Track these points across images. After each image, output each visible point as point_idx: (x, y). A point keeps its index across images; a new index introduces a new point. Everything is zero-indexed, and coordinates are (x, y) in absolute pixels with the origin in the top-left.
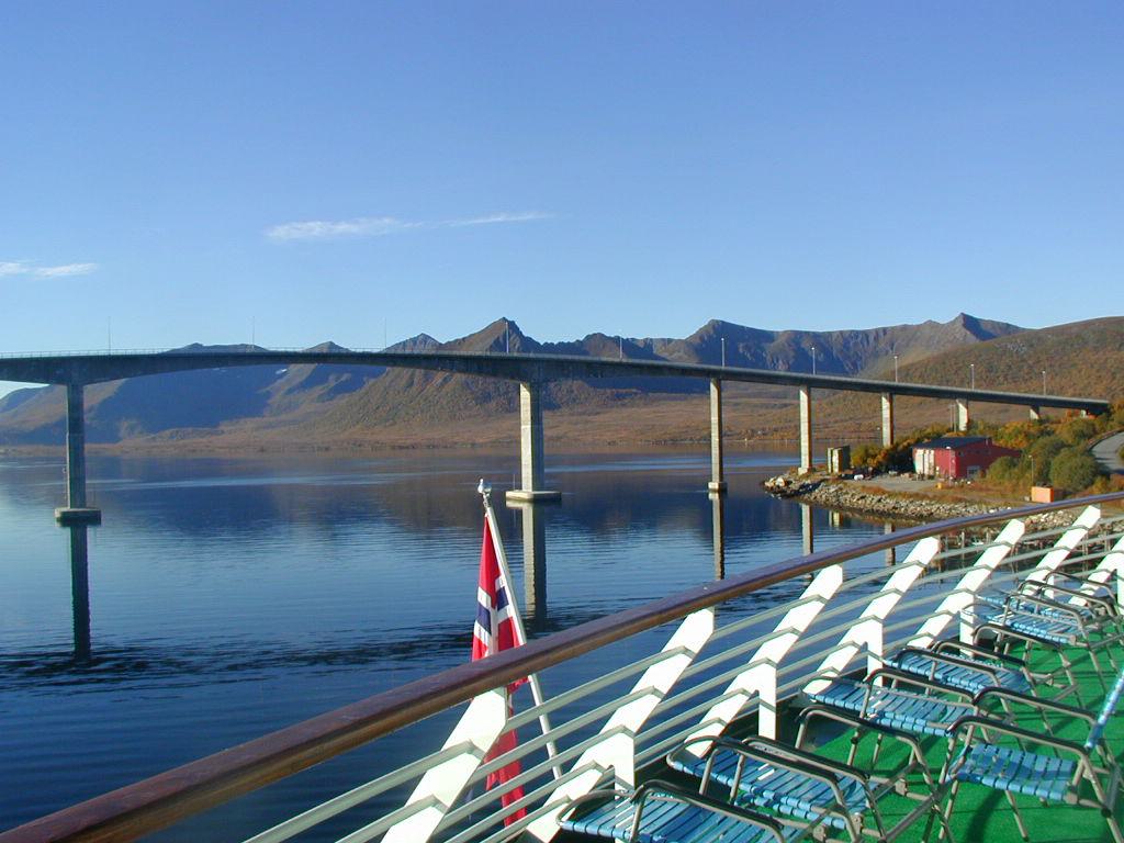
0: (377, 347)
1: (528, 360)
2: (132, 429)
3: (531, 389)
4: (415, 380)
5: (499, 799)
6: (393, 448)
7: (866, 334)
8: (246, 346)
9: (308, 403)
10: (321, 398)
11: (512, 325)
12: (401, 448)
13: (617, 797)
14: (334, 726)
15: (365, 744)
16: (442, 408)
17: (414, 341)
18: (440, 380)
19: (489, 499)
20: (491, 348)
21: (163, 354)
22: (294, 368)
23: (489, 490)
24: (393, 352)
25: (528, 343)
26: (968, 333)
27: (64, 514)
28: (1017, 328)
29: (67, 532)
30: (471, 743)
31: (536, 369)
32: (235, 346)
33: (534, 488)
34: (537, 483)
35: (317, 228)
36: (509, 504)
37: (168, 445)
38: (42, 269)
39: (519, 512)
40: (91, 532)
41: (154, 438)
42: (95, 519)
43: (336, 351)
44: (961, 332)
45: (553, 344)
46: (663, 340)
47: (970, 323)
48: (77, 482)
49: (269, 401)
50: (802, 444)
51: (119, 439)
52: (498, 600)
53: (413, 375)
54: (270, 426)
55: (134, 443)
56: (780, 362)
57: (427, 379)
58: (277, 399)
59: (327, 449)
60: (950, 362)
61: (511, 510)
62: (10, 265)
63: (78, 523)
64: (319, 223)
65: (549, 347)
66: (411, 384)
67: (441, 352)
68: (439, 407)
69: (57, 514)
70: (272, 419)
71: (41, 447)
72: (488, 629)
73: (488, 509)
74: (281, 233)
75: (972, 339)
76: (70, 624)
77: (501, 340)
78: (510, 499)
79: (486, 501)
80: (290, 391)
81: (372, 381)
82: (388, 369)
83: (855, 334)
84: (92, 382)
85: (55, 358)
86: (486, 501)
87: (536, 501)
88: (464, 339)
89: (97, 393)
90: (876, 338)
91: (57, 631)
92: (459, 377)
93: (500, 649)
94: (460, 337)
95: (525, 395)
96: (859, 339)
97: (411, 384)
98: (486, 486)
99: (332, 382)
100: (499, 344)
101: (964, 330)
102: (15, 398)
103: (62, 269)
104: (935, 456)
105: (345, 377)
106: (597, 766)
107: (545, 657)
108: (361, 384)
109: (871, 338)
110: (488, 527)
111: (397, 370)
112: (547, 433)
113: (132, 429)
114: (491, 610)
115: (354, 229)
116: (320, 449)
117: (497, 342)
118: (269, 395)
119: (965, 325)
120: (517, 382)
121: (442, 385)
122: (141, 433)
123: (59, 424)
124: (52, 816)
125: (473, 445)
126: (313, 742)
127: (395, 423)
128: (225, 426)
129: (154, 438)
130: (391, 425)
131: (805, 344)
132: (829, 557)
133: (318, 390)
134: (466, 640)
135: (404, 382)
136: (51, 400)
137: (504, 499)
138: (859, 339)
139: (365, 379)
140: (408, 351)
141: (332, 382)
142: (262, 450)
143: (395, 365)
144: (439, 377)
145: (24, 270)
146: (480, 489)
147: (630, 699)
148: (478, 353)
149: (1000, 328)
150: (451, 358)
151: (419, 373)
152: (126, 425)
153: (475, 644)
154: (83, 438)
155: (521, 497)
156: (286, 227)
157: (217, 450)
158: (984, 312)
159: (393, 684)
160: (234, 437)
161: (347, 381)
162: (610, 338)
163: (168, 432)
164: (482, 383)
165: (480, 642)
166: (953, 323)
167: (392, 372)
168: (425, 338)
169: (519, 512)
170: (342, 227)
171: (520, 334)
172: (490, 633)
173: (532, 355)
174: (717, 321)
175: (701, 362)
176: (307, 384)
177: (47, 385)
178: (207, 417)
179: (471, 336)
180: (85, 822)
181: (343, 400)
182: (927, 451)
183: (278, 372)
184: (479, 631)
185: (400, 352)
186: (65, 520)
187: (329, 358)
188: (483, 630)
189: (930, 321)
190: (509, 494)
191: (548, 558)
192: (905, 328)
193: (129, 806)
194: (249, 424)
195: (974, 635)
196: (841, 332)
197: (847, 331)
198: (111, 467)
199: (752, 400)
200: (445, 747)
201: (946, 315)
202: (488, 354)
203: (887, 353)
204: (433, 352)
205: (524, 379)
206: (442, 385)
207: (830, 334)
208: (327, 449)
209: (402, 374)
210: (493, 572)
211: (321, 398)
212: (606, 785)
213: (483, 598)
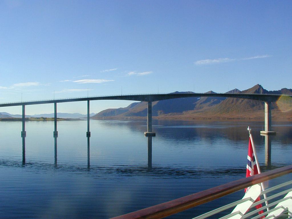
0: (224, 92)
1: (266, 96)
2: (161, 113)
3: (268, 104)
4: (234, 101)
5: (258, 213)
6: (228, 119)
8: (190, 92)
9: (206, 107)
10: (209, 106)
11: (260, 86)
12: (230, 119)
13: (289, 217)
14: (217, 191)
15: (230, 194)
16: (241, 108)
17: (234, 90)
18: (241, 101)
19: (250, 132)
20: (255, 92)
21: (169, 94)
22: (202, 98)
23: (251, 129)
24: (228, 93)
25: (265, 91)
27: (147, 133)
29: (147, 138)
30: (251, 198)
31: (269, 98)
32: (187, 92)
33: (268, 131)
34: (269, 129)
35: (207, 61)
36: (261, 135)
37: (170, 117)
38: (139, 73)
39: (264, 137)
40: (153, 138)
41: (166, 115)
42: (154, 135)
43: (213, 93)
45: (272, 91)
48: (150, 126)
49: (195, 106)
50: (265, 127)
51: (158, 115)
52: (253, 159)
53: (233, 99)
54: (196, 113)
55: (160, 116)
57: (237, 101)
58: (197, 106)
59: (210, 119)
61: (262, 136)
62: (132, 72)
63: (150, 136)
64: (208, 60)
65: (271, 92)
66: (233, 102)
67: (241, 94)
68: (240, 108)
69: (145, 133)
70: (196, 111)
71: (139, 117)
72: (251, 167)
73: (250, 135)
74: (198, 63)
76: (147, 160)
78: (261, 133)
79: (250, 132)
80: (201, 104)
81: (223, 101)
82: (227, 98)
85: (136, 95)
86: (250, 132)
87: (269, 134)
88: (247, 90)
89: (154, 103)
91: (144, 161)
92: (246, 100)
93: (254, 174)
95: (266, 105)
97: (233, 102)
98: (250, 128)
99: (212, 101)
102: (133, 105)
103: (144, 73)
105: (215, 100)
106: (282, 207)
107: (272, 176)
108: (219, 102)
110: (250, 140)
111: (229, 98)
112: (272, 115)
113: (161, 113)
114: (251, 162)
115: (218, 61)
116: (209, 119)
117: (256, 91)
118: (195, 105)
120: (263, 102)
121: (241, 102)
122: (163, 114)
123: (145, 111)
124: (145, 209)
125: (249, 118)
126: (212, 195)
127: (228, 112)
128: (184, 112)
129: (166, 115)
130: (227, 113)
133: (208, 103)
134: (244, 171)
135: (231, 102)
136: (145, 105)
137: (260, 133)
139: (220, 100)
140: (232, 93)
141: (212, 101)
142: (194, 119)
143: (229, 97)
144: (240, 100)
145: (135, 74)
146: (248, 129)
147: (265, 192)
148: (252, 94)
150: (243, 95)
151: (235, 99)
152: (159, 112)
153: (247, 172)
154: (151, 115)
155: (264, 133)
156: (200, 61)
157: (182, 118)
159: (230, 181)
160: (187, 115)
161: (216, 101)
163: (169, 114)
164: (252, 101)
165: (249, 170)
167: (228, 99)
168: (237, 90)
169: (264, 137)
170: (214, 61)
171: (263, 88)
172: (251, 168)
173: (266, 94)
176: (205, 102)
177: (140, 101)
178: (180, 110)
179: (249, 89)
180: (157, 210)
181: (215, 106)
183: (198, 99)
184: (248, 167)
185: (230, 93)
186: (147, 135)
187: (212, 95)
188: (249, 167)
190: (261, 132)
193: (167, 207)
194: (190, 112)
198: (156, 122)
200: (243, 199)
202: (254, 94)
204: (239, 94)
205: (266, 101)
206: (241, 102)
208: (210, 119)
209: (231, 99)
210: (252, 152)
211: (209, 106)
212: (285, 213)
213: (249, 158)
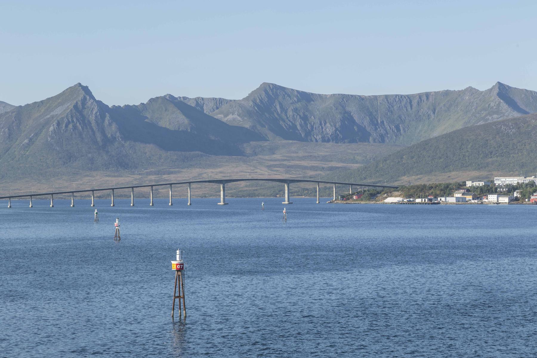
7: (409, 98)
11: (86, 89)
26: (502, 101)
44: (495, 100)
45: (119, 106)
46: (214, 99)
56: (328, 125)
77: (79, 103)
83: (400, 98)
96: (403, 103)
101: (498, 99)
109: (415, 102)
119: (500, 95)
131: (352, 108)
132: (295, 248)
138: (403, 103)
161: (419, 197)
166: (491, 90)
174: (269, 85)
192: (447, 93)
195: (469, 186)
196: (387, 97)
197: (392, 96)
199: (349, 164)
207: (376, 97)
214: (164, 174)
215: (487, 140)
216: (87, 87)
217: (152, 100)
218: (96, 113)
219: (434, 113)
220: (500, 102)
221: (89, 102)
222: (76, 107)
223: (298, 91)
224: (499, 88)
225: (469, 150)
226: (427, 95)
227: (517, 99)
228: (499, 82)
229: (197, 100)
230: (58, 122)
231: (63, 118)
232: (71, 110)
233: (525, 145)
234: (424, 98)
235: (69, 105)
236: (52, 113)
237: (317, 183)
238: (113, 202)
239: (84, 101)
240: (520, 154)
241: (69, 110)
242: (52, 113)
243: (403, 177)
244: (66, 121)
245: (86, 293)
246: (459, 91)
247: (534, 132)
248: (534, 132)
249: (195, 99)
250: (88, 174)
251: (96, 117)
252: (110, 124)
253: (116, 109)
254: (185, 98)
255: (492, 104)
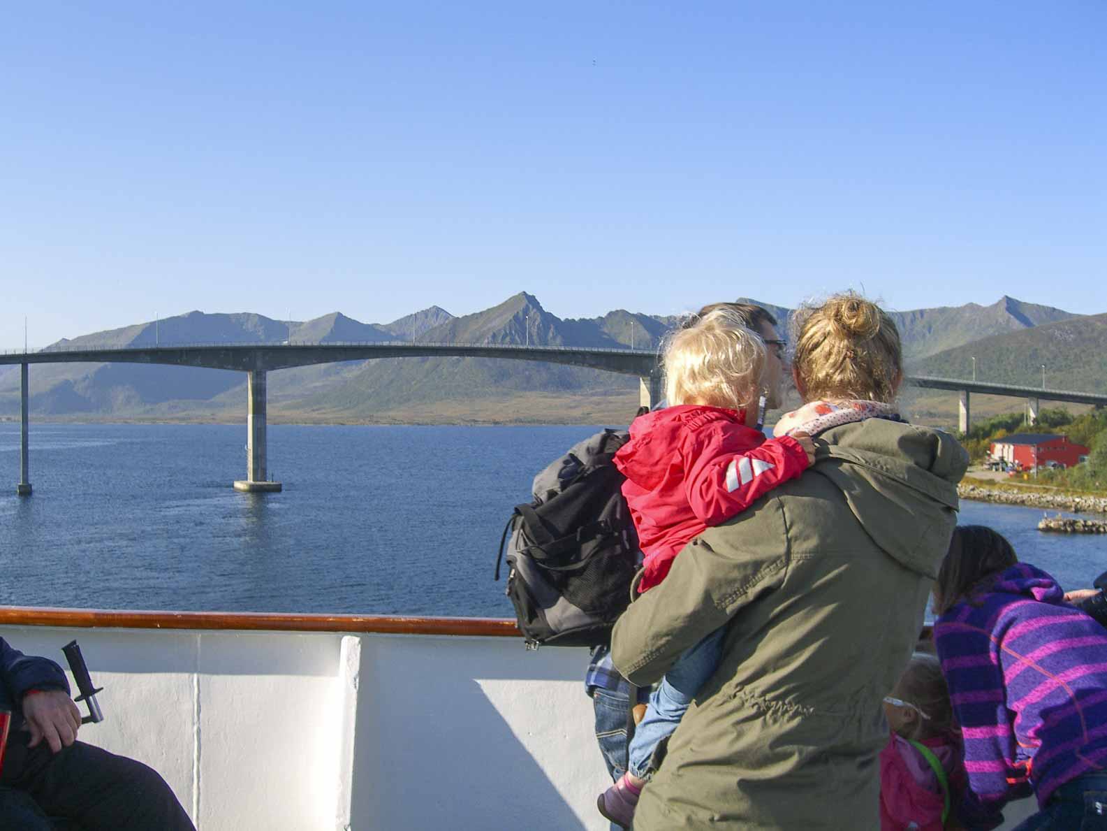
11: (532, 300)
26: (1012, 317)
28: (1063, 312)
44: (1003, 315)
47: (1012, 306)
60: (988, 348)
75: (1017, 325)
77: (521, 314)
84: (273, 369)
90: (912, 321)
94: (478, 312)
100: (519, 322)
101: (1007, 314)
104: (1014, 451)
109: (908, 322)
119: (1008, 309)
149: (1046, 313)
158: (1028, 296)
162: (633, 315)
166: (996, 305)
168: (64, 340)
175: (565, 345)
182: (1006, 446)
189: (972, 303)
191: (20, 385)
192: (943, 311)
201: (988, 298)
203: (924, 335)
214: (611, 395)
215: (1036, 350)
216: (534, 297)
217: (610, 314)
218: (539, 324)
219: (930, 332)
220: (1009, 318)
221: (532, 312)
222: (516, 317)
223: (778, 308)
224: (1008, 303)
225: (1012, 362)
226: (922, 312)
227: (1027, 314)
228: (1007, 297)
229: (669, 318)
230: (494, 334)
231: (500, 330)
232: (510, 321)
233: (1093, 356)
234: (918, 316)
235: (510, 316)
236: (489, 325)
237: (961, 395)
238: (259, 458)
239: (526, 311)
240: (1087, 368)
241: (508, 321)
242: (489, 325)
243: (920, 399)
244: (503, 332)
245: (856, 305)
246: (958, 308)
247: (1102, 338)
248: (1102, 338)
249: (668, 318)
250: (521, 394)
251: (539, 328)
252: (554, 338)
253: (570, 322)
254: (656, 317)
255: (1000, 320)
